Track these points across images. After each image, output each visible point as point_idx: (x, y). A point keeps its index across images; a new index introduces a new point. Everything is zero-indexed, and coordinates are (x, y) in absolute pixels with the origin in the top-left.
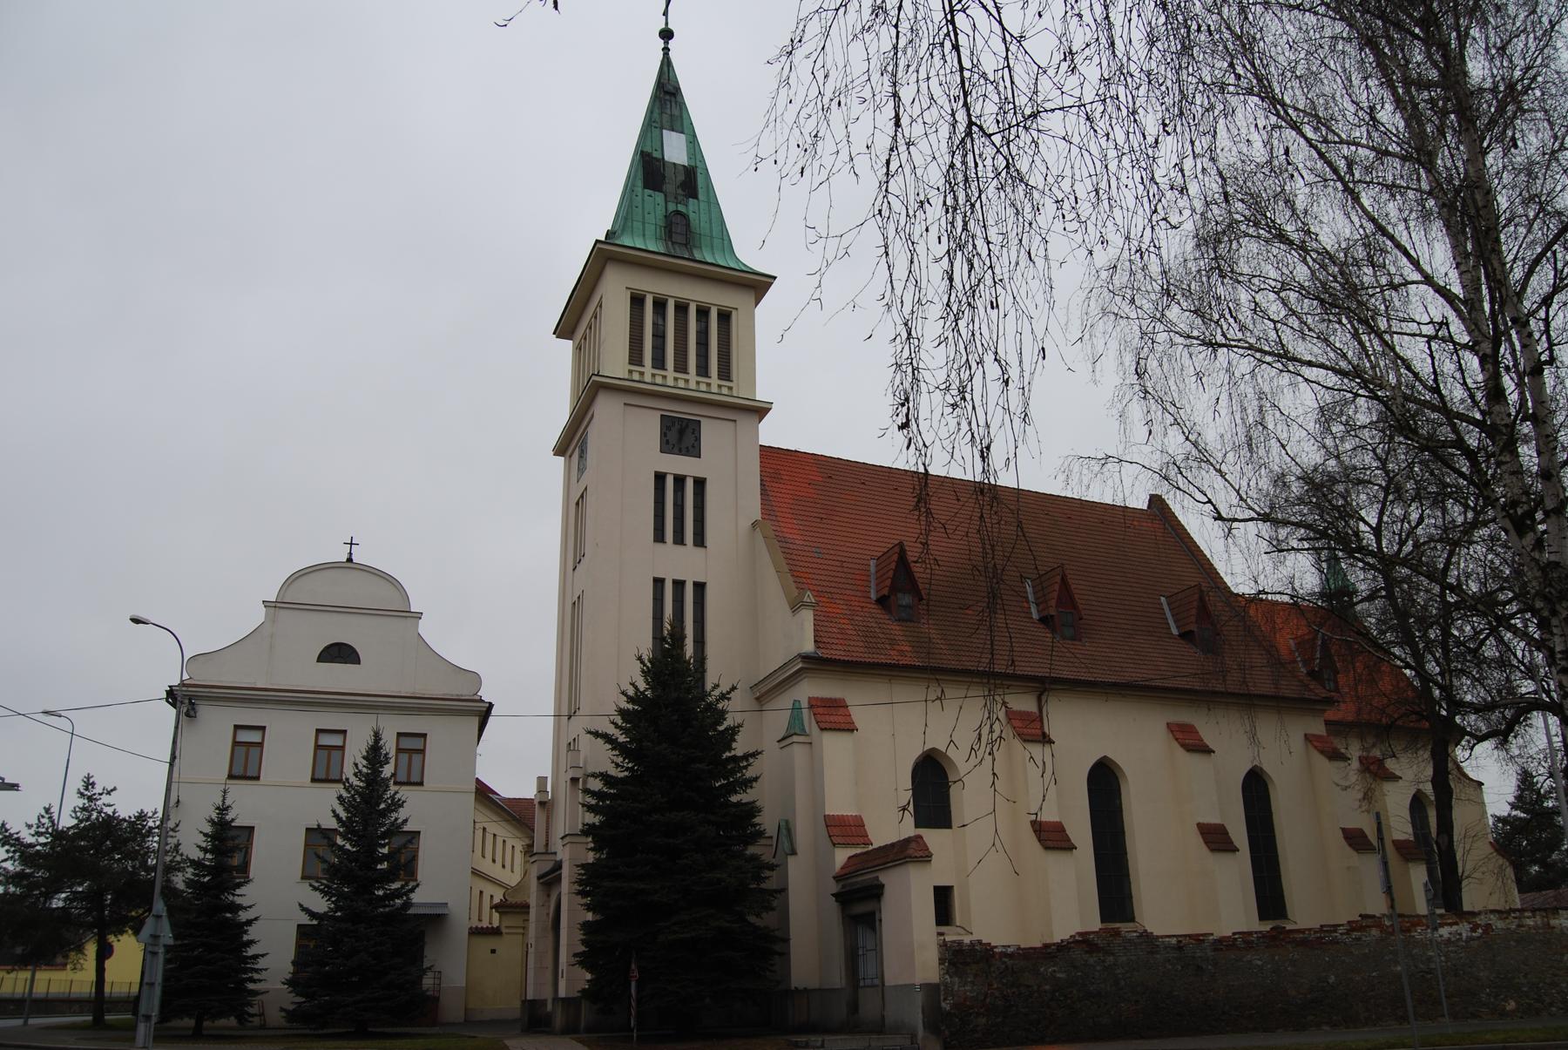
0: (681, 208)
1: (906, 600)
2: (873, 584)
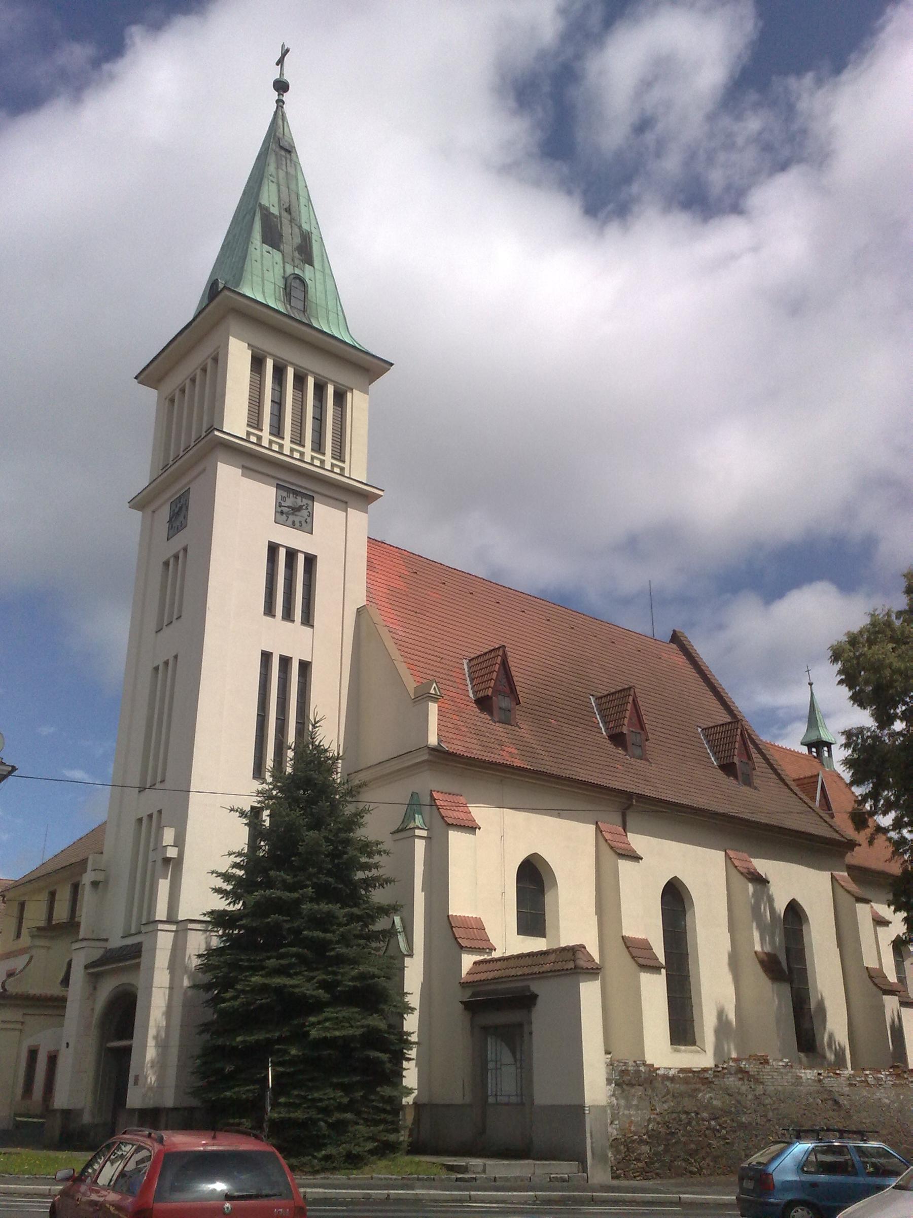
0: (297, 271)
1: (504, 702)
2: (468, 682)
